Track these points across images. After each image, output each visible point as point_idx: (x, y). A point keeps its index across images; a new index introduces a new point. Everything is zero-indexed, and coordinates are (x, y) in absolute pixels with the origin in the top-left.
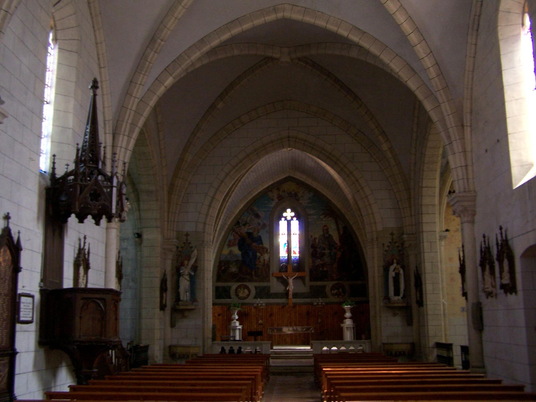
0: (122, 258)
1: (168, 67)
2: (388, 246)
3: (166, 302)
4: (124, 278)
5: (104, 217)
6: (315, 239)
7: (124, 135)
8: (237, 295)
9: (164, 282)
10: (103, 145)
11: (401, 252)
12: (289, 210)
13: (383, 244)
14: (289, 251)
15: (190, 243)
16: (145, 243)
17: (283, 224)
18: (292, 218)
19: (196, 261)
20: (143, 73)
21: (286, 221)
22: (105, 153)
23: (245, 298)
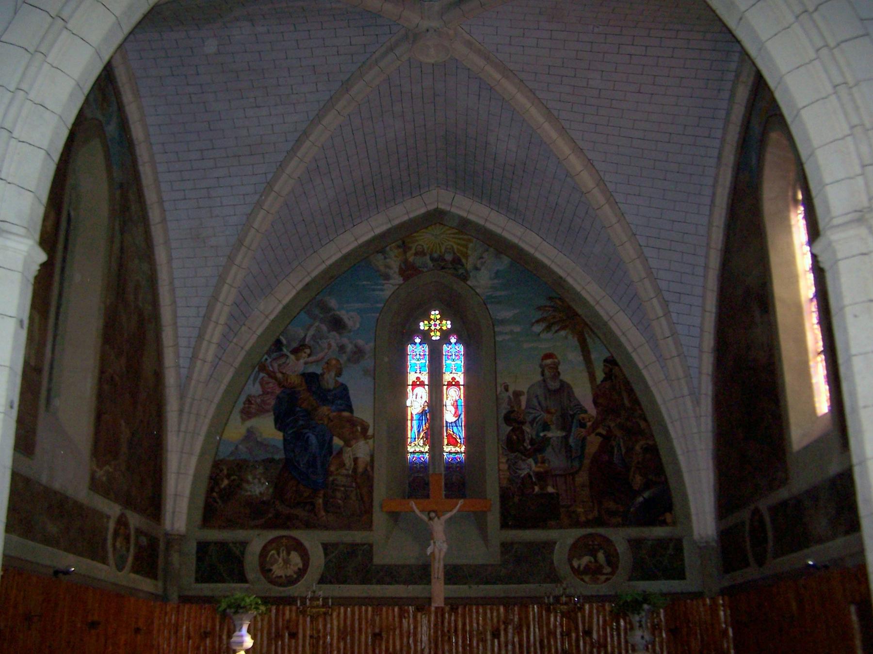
6: (517, 394)
12: (435, 314)
18: (445, 336)
23: (291, 581)
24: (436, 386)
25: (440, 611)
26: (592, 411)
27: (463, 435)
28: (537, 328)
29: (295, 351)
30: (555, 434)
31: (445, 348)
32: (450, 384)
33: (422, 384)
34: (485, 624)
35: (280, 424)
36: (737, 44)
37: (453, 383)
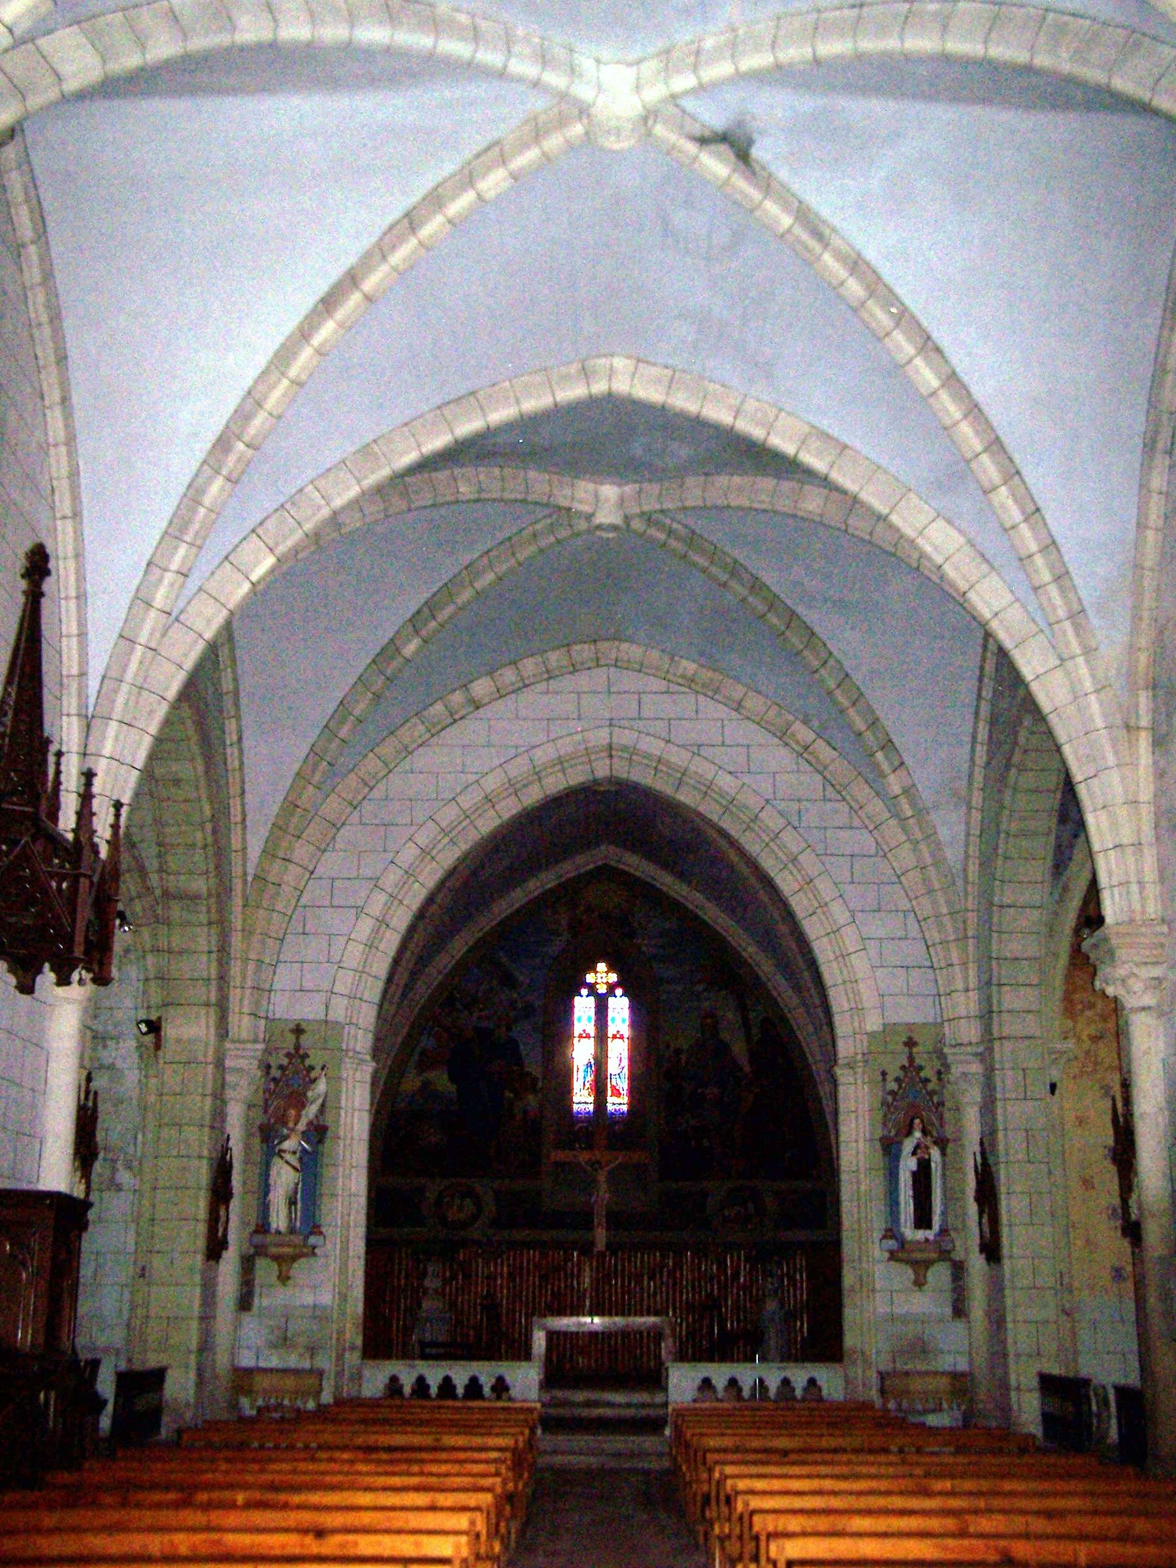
0: (96, 1093)
1: (261, 524)
2: (897, 1080)
3: (226, 1229)
4: (101, 1155)
5: (47, 966)
6: (678, 1051)
7: (241, 1013)
8: (465, 1225)
9: (222, 1170)
10: (53, 748)
11: (935, 1099)
12: (602, 967)
13: (884, 1074)
14: (600, 1088)
15: (306, 1056)
16: (170, 1049)
17: (583, 1007)
18: (611, 988)
19: (322, 1109)
20: (188, 538)
21: (592, 999)
22: (58, 772)
23: (465, 1225)
24: (601, 1038)
25: (602, 1255)
26: (747, 1069)
27: (626, 1087)
28: (700, 987)
29: (467, 1007)
30: (712, 1091)
31: (611, 1000)
32: (614, 1037)
33: (588, 1036)
34: (642, 1267)
35: (452, 1079)
36: (1057, 756)
37: (618, 1036)
